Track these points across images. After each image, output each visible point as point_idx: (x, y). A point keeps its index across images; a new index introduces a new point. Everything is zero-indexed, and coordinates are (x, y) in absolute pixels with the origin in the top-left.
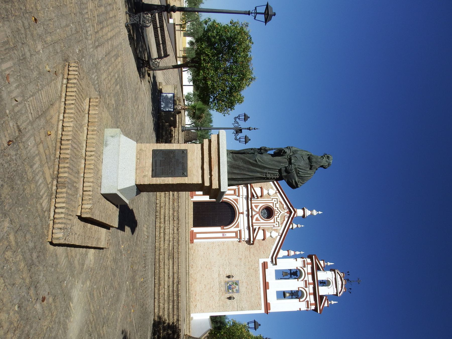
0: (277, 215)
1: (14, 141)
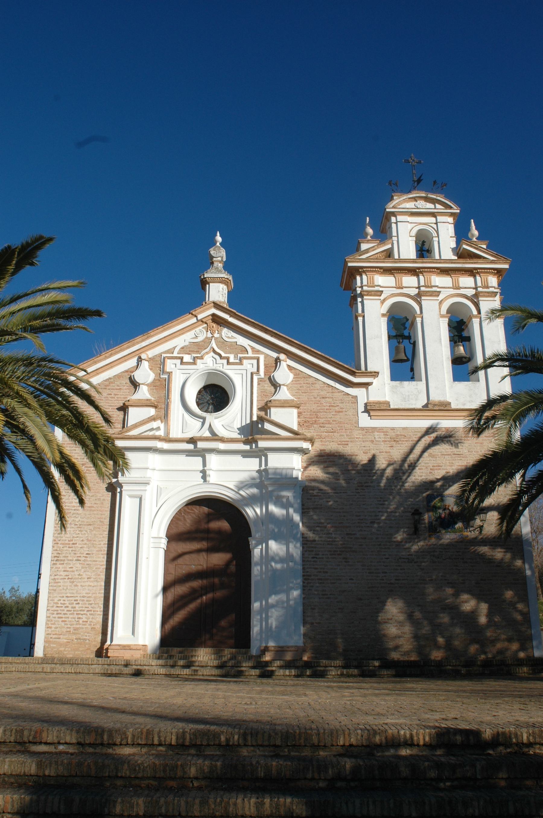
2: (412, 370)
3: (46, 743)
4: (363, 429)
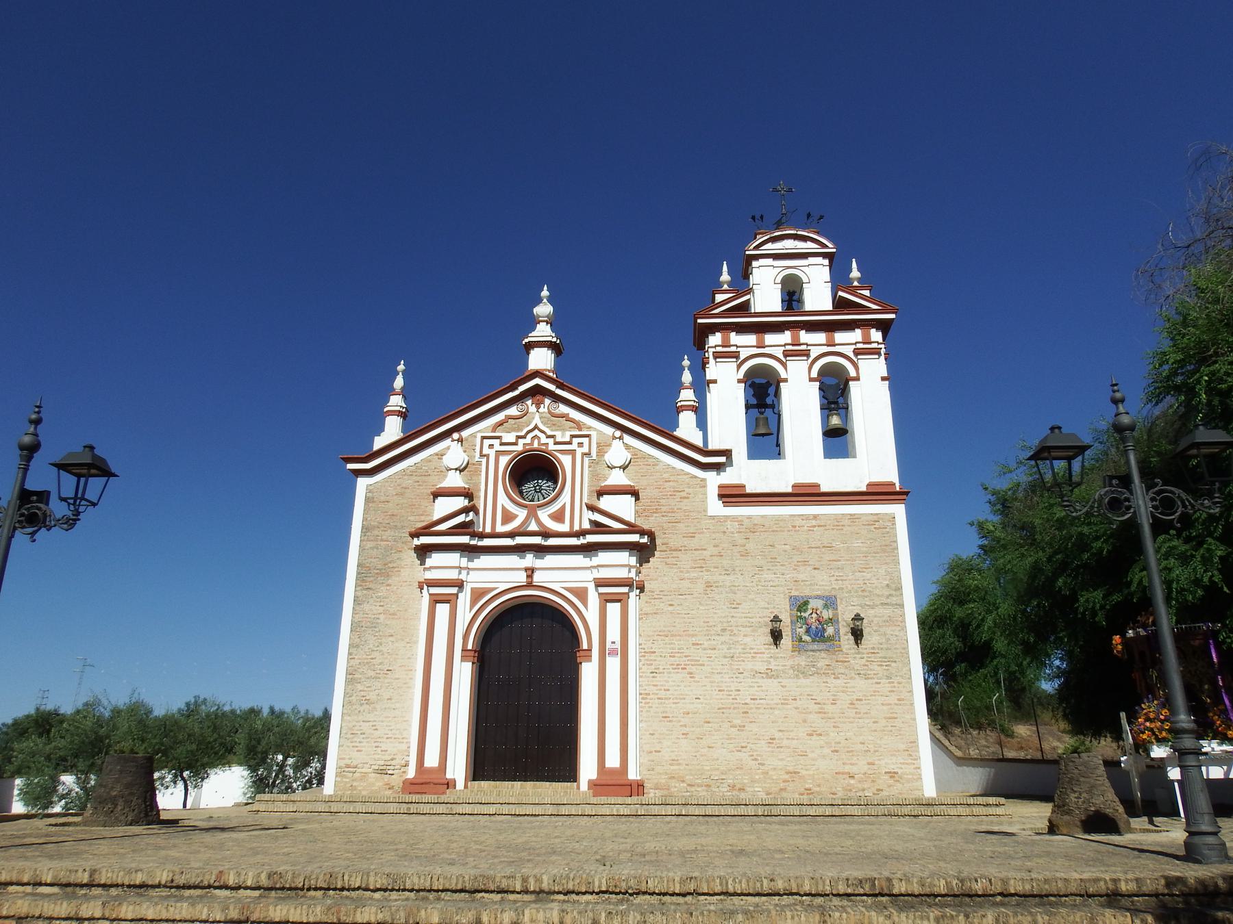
0: (544, 440)
2: (778, 445)
3: (46, 885)
4: (713, 517)
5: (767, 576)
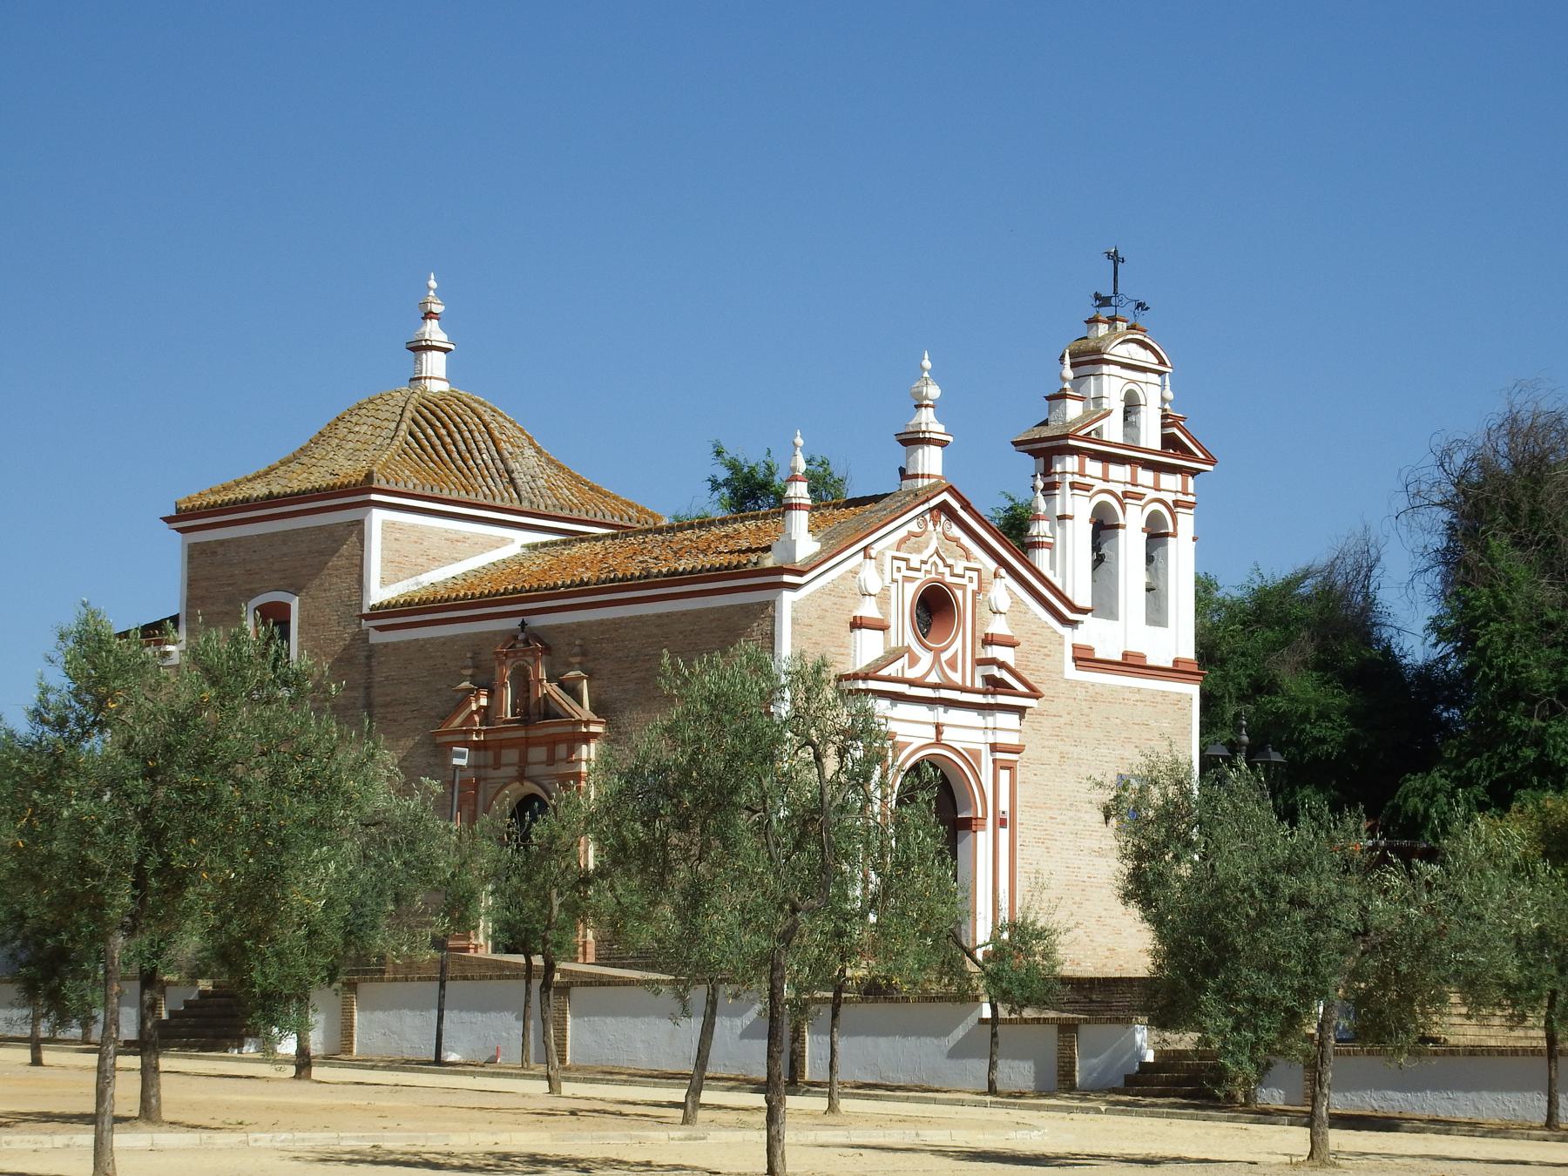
0: (941, 569)
1: (530, 788)
5: (1103, 751)
